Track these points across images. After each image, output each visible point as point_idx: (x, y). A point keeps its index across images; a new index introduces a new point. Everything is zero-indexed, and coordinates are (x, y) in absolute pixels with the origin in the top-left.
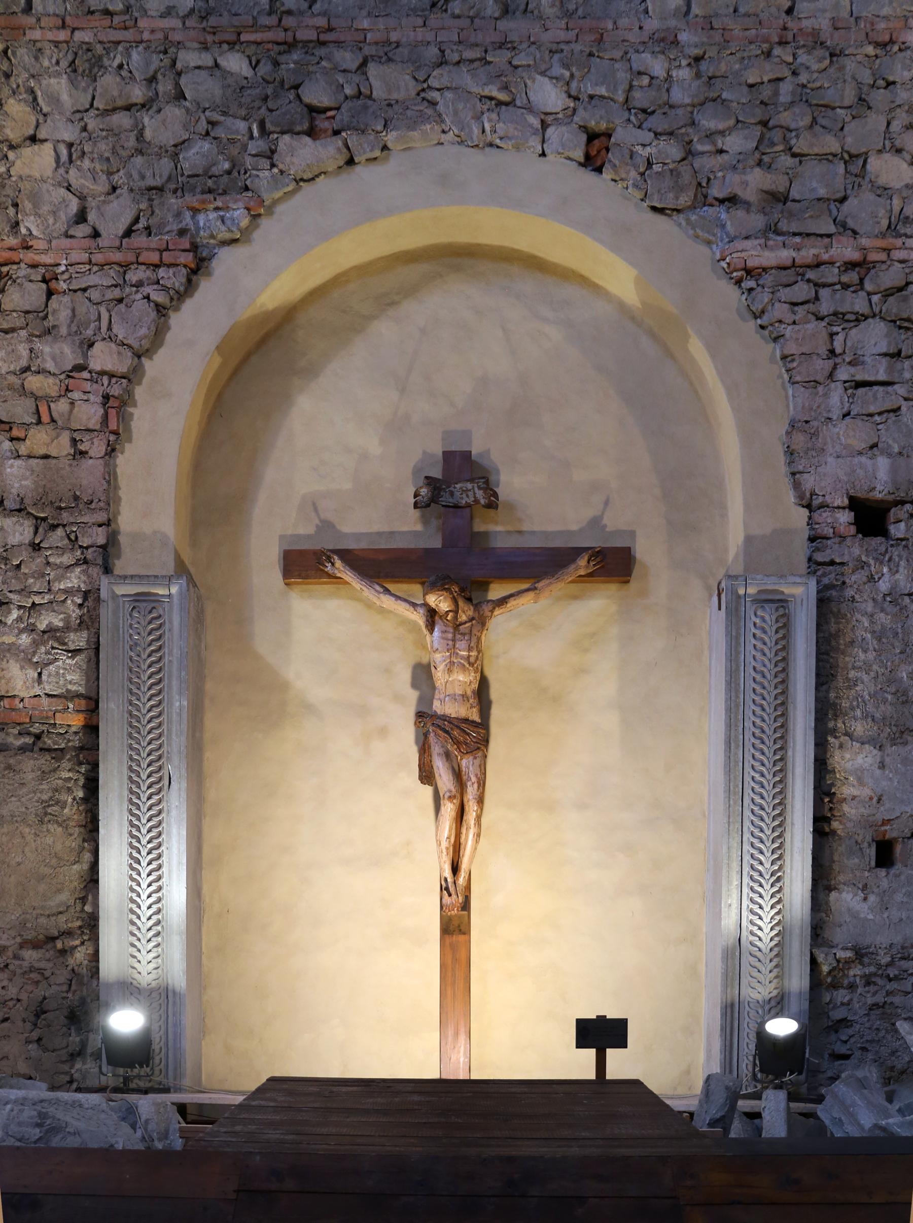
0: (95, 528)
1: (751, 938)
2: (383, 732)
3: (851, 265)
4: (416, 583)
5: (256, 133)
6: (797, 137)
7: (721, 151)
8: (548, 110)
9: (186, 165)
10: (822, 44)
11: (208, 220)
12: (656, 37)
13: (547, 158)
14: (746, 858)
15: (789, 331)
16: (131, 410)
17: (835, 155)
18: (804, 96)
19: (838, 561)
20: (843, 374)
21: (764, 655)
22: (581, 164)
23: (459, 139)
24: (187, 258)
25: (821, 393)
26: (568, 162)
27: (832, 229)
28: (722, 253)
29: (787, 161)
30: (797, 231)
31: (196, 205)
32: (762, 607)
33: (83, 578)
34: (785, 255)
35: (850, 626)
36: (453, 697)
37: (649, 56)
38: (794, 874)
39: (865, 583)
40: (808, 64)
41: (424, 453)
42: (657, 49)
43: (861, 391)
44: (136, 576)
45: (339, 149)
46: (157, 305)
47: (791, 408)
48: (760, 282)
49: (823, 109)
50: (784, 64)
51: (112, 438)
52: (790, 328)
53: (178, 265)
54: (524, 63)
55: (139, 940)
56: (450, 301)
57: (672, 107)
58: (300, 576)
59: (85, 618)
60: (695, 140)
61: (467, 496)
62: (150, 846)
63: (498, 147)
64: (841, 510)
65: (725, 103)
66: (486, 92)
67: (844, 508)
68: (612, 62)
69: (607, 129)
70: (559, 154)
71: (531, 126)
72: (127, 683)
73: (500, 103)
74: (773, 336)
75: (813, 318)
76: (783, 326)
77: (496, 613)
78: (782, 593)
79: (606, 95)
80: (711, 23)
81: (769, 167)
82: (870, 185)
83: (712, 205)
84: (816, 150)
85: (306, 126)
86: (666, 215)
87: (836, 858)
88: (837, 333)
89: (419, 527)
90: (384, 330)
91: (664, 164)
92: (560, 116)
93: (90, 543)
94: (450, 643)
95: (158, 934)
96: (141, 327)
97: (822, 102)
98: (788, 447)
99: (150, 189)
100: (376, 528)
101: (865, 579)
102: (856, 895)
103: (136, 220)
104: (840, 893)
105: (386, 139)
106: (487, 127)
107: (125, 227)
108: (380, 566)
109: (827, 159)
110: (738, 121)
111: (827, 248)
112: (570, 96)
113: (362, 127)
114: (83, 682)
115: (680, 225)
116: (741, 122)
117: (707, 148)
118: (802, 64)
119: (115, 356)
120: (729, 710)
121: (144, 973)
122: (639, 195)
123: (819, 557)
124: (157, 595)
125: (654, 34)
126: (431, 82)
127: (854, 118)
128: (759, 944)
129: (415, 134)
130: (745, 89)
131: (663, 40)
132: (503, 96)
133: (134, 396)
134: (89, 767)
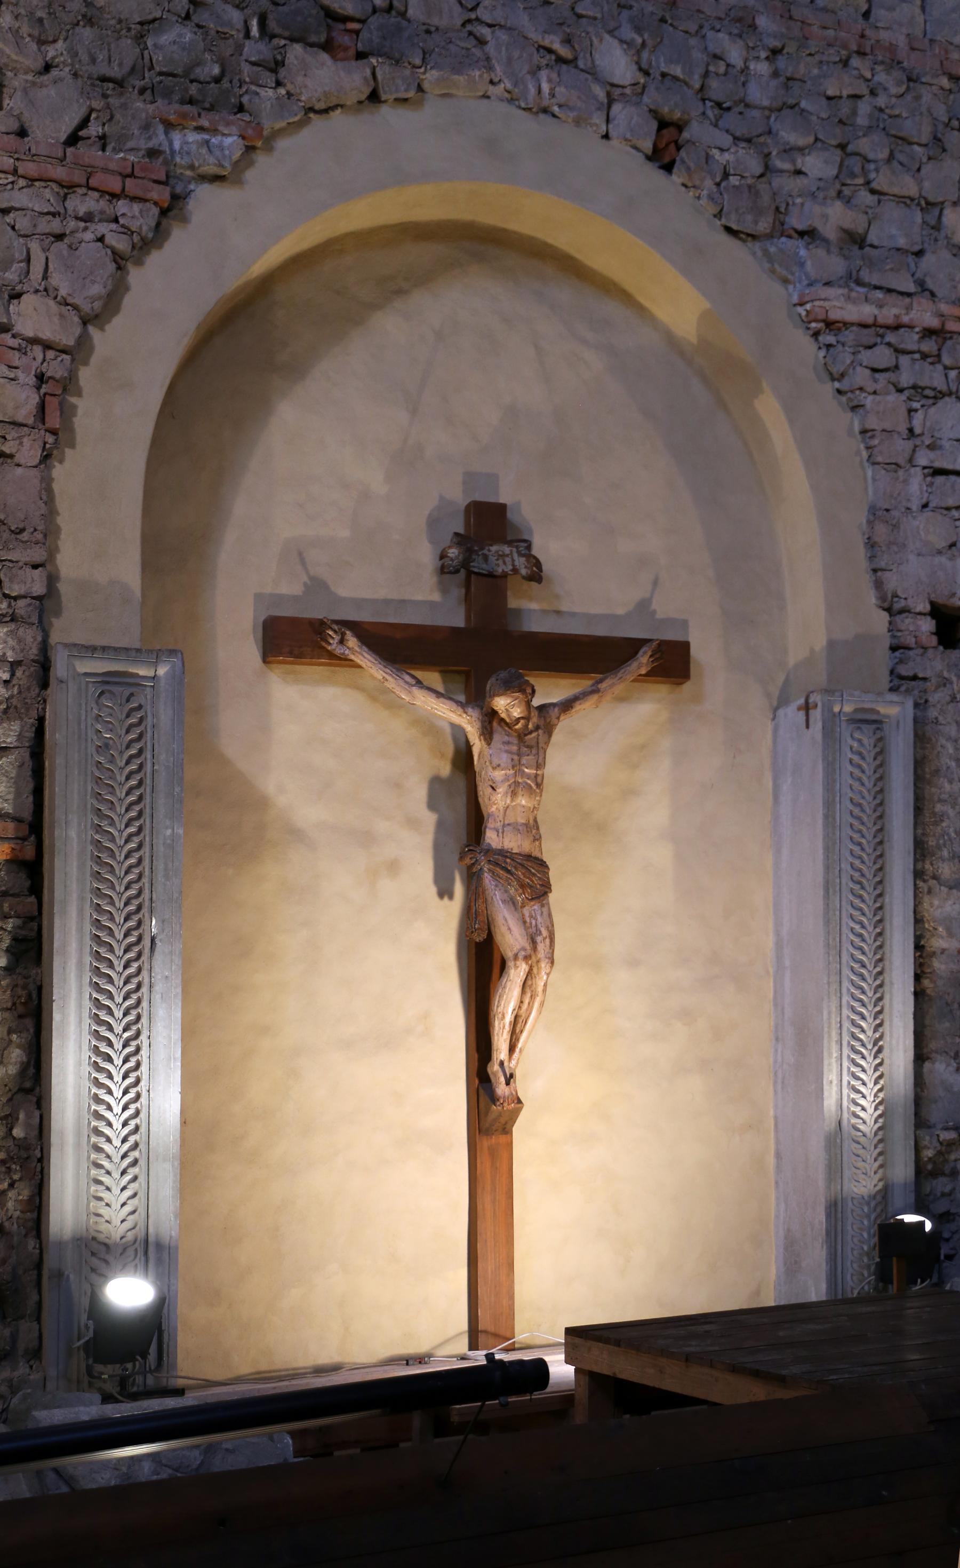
0: (28, 569)
1: (854, 1121)
2: (393, 867)
3: (929, 333)
4: (435, 671)
5: (255, 31)
6: (877, 170)
7: (799, 172)
8: (615, 81)
9: (158, 57)
10: (899, 63)
11: (185, 141)
12: (732, 14)
13: (611, 142)
14: (846, 1024)
15: (869, 401)
16: (73, 400)
17: (912, 200)
18: (881, 121)
19: (920, 675)
20: (923, 459)
21: (863, 784)
22: (649, 158)
23: (507, 95)
24: (161, 194)
25: (901, 479)
26: (633, 151)
27: (912, 288)
28: (801, 296)
29: (865, 198)
30: (878, 284)
31: (172, 118)
32: (859, 728)
33: (11, 642)
34: (867, 312)
35: (936, 752)
36: (515, 827)
37: (727, 37)
38: (894, 1042)
39: (948, 703)
40: (887, 85)
41: (441, 498)
42: (736, 31)
43: (940, 479)
44: (109, 647)
45: (365, 79)
46: (115, 252)
47: (870, 493)
48: (842, 339)
49: (900, 142)
50: (862, 80)
51: (50, 439)
52: (870, 398)
53: (146, 200)
54: (590, 13)
55: (108, 1173)
56: (468, 301)
57: (747, 106)
58: (291, 654)
59: (14, 701)
60: (774, 153)
61: (505, 563)
62: (126, 1035)
63: (554, 116)
64: (923, 617)
65: (805, 114)
66: (546, 43)
67: (924, 614)
68: (687, 36)
69: (679, 119)
70: (626, 140)
71: (595, 98)
72: (91, 801)
73: (561, 60)
74: (852, 404)
75: (893, 390)
76: (864, 395)
77: (562, 718)
78: (878, 712)
79: (681, 77)
80: (789, 11)
81: (848, 202)
82: (945, 242)
83: (790, 237)
84: (896, 190)
85: (323, 38)
86: (740, 239)
87: (927, 1022)
88: (916, 411)
89: (436, 597)
90: (390, 326)
91: (742, 177)
92: (628, 91)
93: (22, 592)
94: (516, 757)
95: (135, 1163)
96: (93, 282)
97: (900, 134)
98: (869, 538)
99: (104, 79)
100: (382, 594)
101: (948, 698)
102: (948, 1065)
103: (85, 123)
104: (933, 1063)
105: (422, 77)
106: (546, 87)
107: (70, 130)
108: (402, 647)
109: (905, 203)
110: (817, 139)
111: (909, 308)
112: (640, 69)
113: (397, 55)
114: (11, 797)
115: (754, 254)
116: (821, 140)
117: (787, 166)
118: (880, 84)
119: (56, 320)
120: (827, 849)
121: (116, 1221)
122: (713, 209)
123: (904, 670)
124: (137, 675)
125: (730, 10)
126: (480, 12)
127: (929, 159)
128: (862, 1127)
129: (461, 79)
130: (824, 101)
131: (739, 20)
132: (564, 52)
133: (77, 380)
134: (18, 922)
